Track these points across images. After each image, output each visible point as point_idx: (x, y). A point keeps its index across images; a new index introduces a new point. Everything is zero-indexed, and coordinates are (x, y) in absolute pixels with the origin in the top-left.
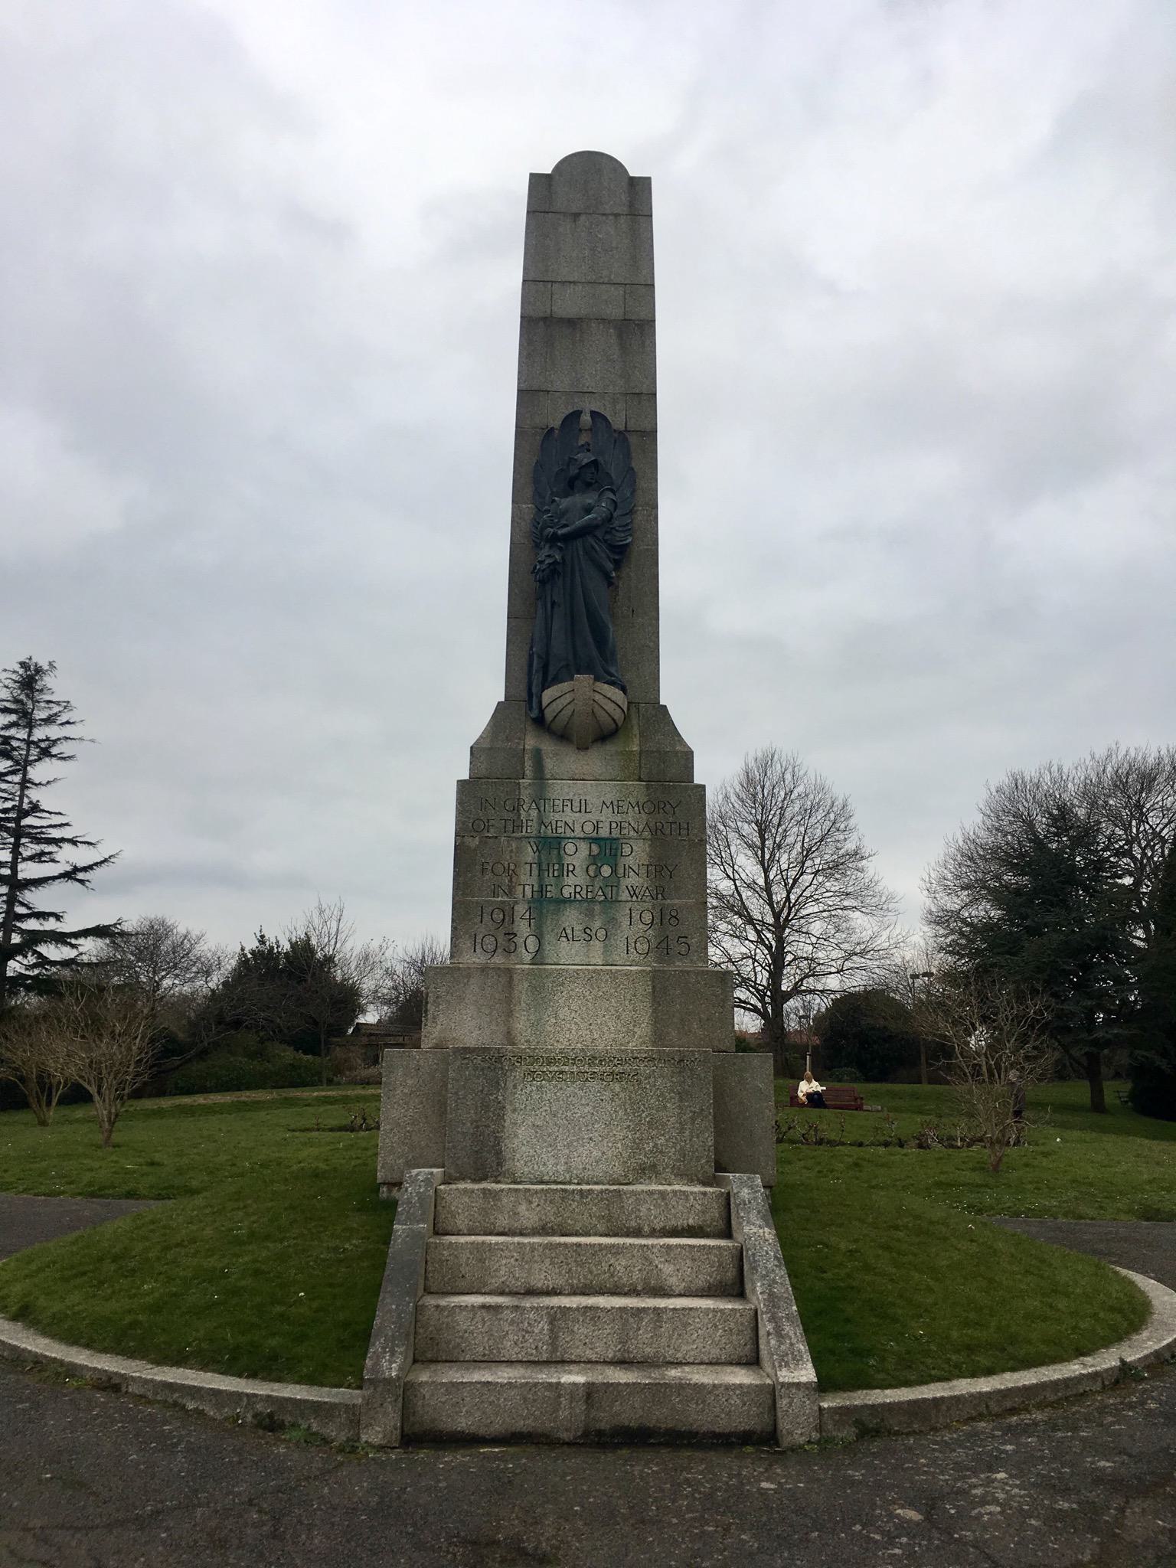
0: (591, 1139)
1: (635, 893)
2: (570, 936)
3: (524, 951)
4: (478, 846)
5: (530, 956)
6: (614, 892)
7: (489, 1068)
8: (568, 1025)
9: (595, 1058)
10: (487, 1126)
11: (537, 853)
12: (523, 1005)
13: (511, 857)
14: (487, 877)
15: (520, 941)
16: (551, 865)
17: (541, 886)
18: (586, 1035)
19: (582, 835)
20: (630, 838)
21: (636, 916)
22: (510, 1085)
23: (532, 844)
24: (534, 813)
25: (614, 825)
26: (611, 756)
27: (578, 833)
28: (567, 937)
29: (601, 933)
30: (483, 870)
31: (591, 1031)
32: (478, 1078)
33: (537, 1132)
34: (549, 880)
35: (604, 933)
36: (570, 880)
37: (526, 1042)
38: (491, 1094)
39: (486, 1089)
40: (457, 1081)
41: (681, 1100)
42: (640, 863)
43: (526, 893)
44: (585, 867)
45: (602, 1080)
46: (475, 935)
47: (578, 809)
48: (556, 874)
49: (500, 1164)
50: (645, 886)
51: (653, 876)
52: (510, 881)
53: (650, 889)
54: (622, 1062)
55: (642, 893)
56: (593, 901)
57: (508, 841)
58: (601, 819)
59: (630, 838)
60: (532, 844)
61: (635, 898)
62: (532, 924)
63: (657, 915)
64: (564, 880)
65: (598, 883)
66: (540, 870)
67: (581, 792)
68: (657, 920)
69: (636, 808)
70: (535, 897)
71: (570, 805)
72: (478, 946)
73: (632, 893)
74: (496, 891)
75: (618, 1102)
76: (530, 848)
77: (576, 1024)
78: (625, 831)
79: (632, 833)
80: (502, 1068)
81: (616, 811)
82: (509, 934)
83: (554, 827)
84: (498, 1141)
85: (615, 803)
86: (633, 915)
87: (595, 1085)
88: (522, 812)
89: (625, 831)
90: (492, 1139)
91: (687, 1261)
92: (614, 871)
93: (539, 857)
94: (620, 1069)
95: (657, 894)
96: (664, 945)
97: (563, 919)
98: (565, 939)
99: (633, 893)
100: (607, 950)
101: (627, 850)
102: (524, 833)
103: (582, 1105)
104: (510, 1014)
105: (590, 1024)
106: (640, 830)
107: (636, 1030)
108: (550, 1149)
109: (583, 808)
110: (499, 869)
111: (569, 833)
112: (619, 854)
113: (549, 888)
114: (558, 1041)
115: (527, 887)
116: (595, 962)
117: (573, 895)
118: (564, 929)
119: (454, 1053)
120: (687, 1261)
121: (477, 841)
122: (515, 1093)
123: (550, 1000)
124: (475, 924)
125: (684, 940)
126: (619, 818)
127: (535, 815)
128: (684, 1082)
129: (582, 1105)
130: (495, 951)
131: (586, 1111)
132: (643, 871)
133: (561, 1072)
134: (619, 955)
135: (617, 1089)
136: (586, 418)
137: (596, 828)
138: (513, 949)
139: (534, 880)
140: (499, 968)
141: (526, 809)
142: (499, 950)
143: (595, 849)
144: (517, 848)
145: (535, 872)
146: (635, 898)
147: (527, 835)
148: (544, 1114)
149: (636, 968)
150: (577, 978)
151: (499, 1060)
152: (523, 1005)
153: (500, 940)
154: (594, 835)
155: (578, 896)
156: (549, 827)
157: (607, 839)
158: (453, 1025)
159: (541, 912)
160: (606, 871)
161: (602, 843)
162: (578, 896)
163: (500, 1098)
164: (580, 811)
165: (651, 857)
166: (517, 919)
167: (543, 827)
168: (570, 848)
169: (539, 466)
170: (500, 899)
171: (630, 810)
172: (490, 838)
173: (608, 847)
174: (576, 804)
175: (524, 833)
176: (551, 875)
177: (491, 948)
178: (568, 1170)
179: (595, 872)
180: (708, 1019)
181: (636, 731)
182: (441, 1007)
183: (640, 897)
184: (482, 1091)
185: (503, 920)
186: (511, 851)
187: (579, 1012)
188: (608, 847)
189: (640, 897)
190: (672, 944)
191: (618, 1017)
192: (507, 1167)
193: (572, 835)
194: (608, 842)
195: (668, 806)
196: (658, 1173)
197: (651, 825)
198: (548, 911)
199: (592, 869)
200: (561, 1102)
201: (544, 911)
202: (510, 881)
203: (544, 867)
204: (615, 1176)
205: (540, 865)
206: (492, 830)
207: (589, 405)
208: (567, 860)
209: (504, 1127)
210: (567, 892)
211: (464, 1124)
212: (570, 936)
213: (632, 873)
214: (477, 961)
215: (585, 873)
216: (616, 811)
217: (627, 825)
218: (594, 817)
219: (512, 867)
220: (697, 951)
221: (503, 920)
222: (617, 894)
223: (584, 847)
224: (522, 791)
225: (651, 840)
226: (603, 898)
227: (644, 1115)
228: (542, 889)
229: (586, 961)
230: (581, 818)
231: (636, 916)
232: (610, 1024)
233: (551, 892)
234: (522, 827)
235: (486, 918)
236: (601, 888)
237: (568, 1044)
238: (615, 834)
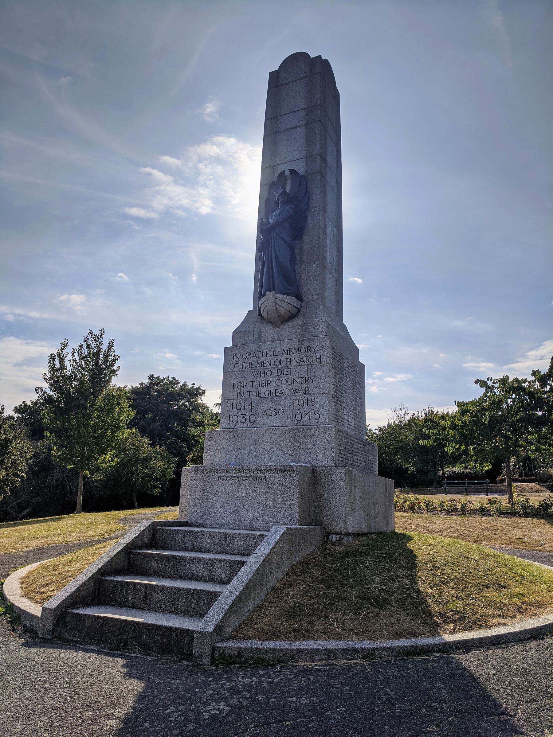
1: (296, 391)
2: (268, 414)
8: (261, 455)
25: (288, 360)
35: (282, 411)
54: (259, 471)
55: (299, 391)
58: (282, 358)
71: (269, 353)
73: (295, 391)
78: (292, 363)
81: (289, 354)
85: (289, 350)
86: (295, 402)
91: (229, 568)
94: (258, 475)
98: (266, 415)
106: (299, 361)
108: (228, 513)
109: (275, 353)
120: (229, 568)
125: (318, 412)
126: (289, 357)
135: (257, 485)
136: (287, 173)
155: (271, 394)
162: (271, 394)
169: (268, 200)
185: (241, 409)
190: (312, 415)
207: (286, 168)
216: (289, 354)
217: (293, 359)
218: (279, 358)
227: (267, 497)
232: (279, 454)
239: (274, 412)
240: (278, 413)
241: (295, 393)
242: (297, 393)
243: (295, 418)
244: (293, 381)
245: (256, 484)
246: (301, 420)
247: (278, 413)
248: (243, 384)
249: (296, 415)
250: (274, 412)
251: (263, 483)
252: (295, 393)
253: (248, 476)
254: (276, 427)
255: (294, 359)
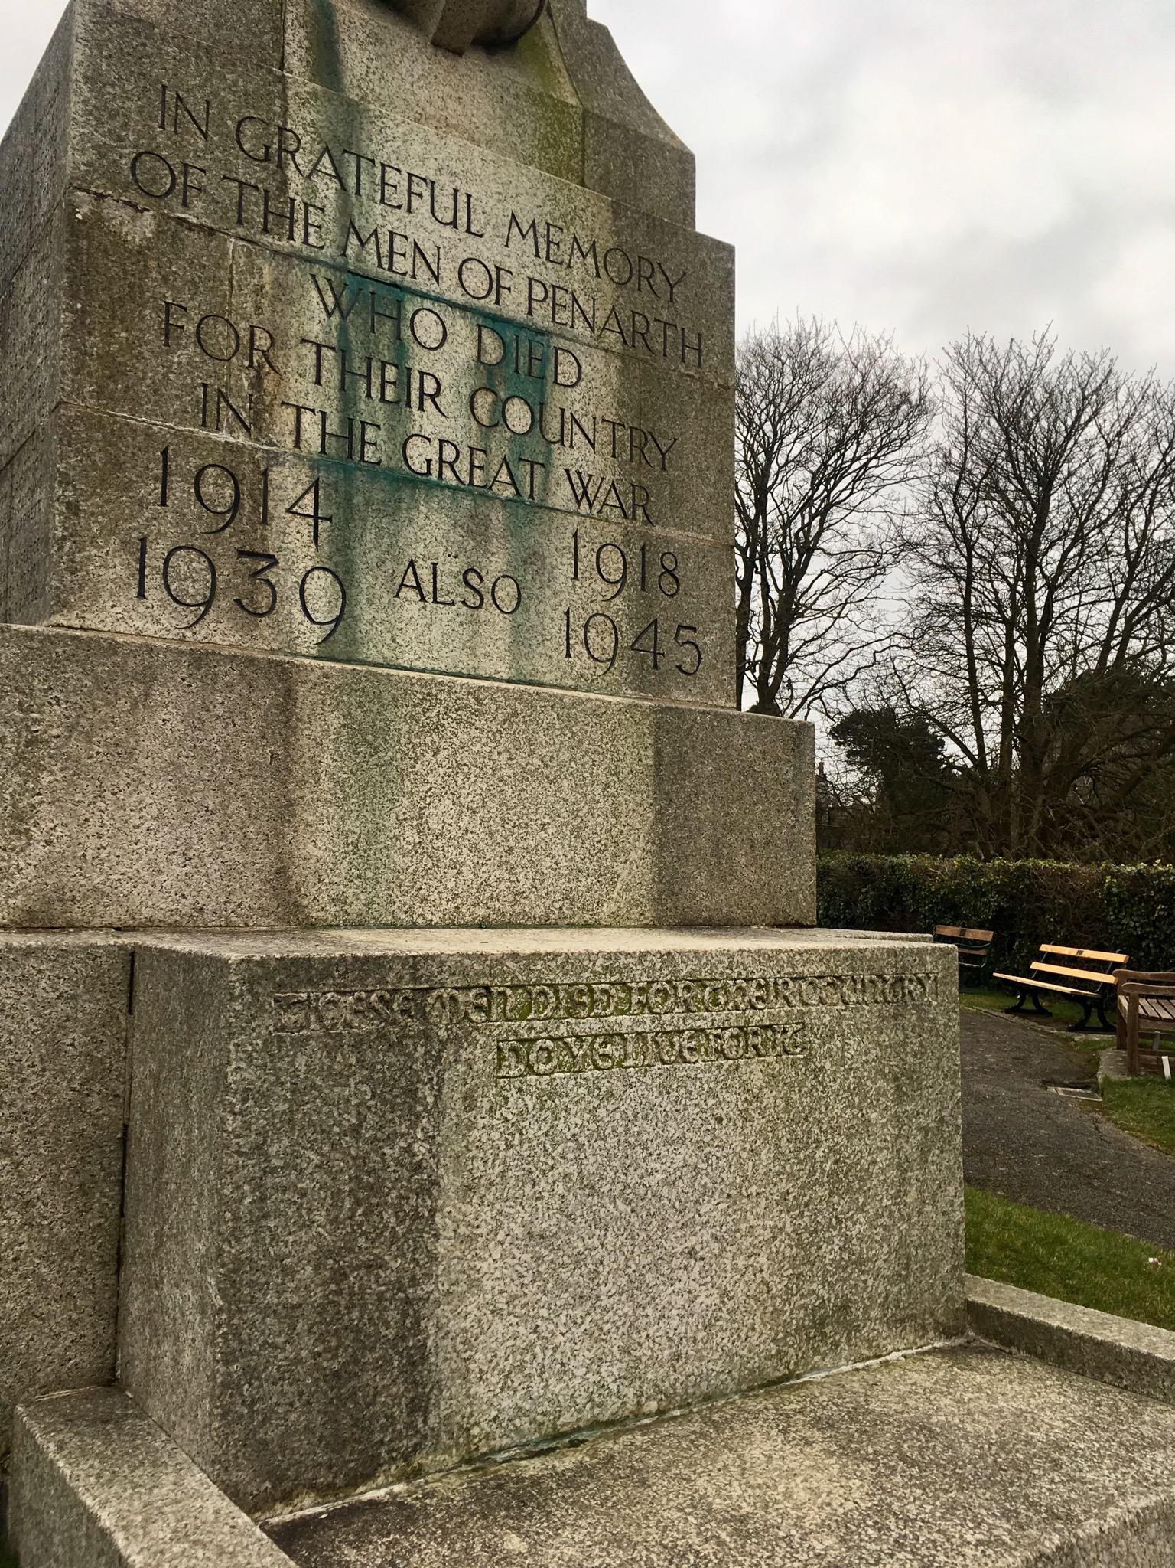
0: (691, 1253)
1: (585, 493)
2: (427, 587)
3: (299, 616)
4: (148, 246)
5: (317, 634)
6: (537, 480)
7: (382, 1036)
9: (701, 983)
10: (374, 1266)
11: (336, 318)
12: (327, 784)
13: (258, 308)
14: (179, 357)
15: (286, 581)
16: (375, 365)
17: (348, 422)
18: (499, 881)
19: (457, 296)
20: (574, 340)
21: (588, 560)
22: (453, 1098)
23: (322, 283)
24: (327, 190)
26: (517, 96)
27: (448, 287)
28: (418, 587)
29: (506, 591)
30: (169, 331)
31: (511, 872)
32: (341, 1078)
33: (539, 1259)
34: (371, 409)
35: (513, 590)
36: (426, 421)
37: (334, 900)
38: (390, 1139)
39: (372, 1119)
40: (263, 1097)
41: (900, 1097)
42: (598, 415)
43: (305, 436)
44: (466, 392)
45: (720, 1053)
46: (143, 541)
47: (449, 218)
48: (390, 395)
49: (419, 1406)
50: (609, 478)
51: (625, 457)
52: (257, 383)
53: (620, 488)
55: (601, 497)
56: (484, 494)
57: (249, 254)
59: (574, 340)
60: (322, 283)
61: (584, 505)
62: (323, 536)
63: (635, 561)
64: (410, 417)
65: (500, 447)
66: (344, 371)
67: (455, 166)
68: (634, 577)
69: (590, 260)
70: (331, 451)
71: (426, 194)
72: (153, 581)
73: (579, 491)
74: (211, 406)
75: (759, 1123)
76: (314, 293)
77: (473, 847)
78: (564, 316)
79: (580, 327)
80: (426, 1036)
82: (253, 555)
83: (385, 249)
84: (413, 1312)
86: (582, 552)
87: (701, 1070)
88: (291, 172)
89: (564, 316)
90: (392, 1315)
92: (538, 421)
93: (343, 331)
95: (634, 506)
96: (647, 642)
97: (409, 533)
98: (412, 595)
99: (582, 496)
100: (519, 640)
101: (567, 370)
102: (298, 242)
103: (668, 1142)
104: (285, 810)
105: (510, 851)
107: (618, 869)
108: (578, 1312)
109: (462, 215)
110: (220, 337)
111: (423, 281)
112: (550, 378)
113: (370, 434)
114: (424, 900)
115: (306, 417)
116: (490, 671)
117: (435, 467)
118: (412, 564)
119: (251, 982)
121: (147, 224)
122: (472, 1126)
123: (403, 773)
124: (142, 504)
125: (687, 635)
126: (549, 274)
127: (332, 194)
128: (904, 1044)
129: (668, 1142)
130: (208, 604)
131: (679, 1161)
132: (603, 437)
133: (609, 1037)
134: (548, 662)
135: (758, 1079)
137: (496, 286)
138: (264, 603)
139: (323, 398)
140: (252, 661)
141: (306, 169)
142: (223, 604)
143: (493, 352)
144: (277, 283)
145: (331, 374)
146: (584, 505)
147: (305, 251)
148: (560, 1189)
149: (619, 699)
150: (475, 713)
151: (417, 1004)
152: (327, 784)
153: (225, 572)
154: (489, 304)
155: (448, 474)
156: (371, 246)
157: (522, 326)
158: (93, 842)
159: (349, 499)
160: (519, 416)
161: (509, 335)
162: (448, 474)
163: (421, 1149)
164: (454, 224)
165: (621, 404)
166: (278, 511)
167: (354, 240)
168: (427, 327)
170: (223, 436)
171: (576, 260)
172: (191, 227)
173: (524, 349)
174: (444, 200)
175: (298, 242)
176: (375, 393)
177: (195, 590)
178: (632, 1375)
179: (492, 412)
180: (768, 843)
181: (558, 62)
182: (45, 778)
183: (597, 506)
184: (355, 1131)
185: (236, 506)
186: (259, 290)
187: (482, 812)
188: (524, 349)
189: (597, 506)
190: (666, 642)
191: (577, 831)
192: (444, 1409)
193: (434, 288)
194: (523, 334)
195: (659, 278)
196: (851, 1328)
197: (622, 316)
198: (368, 503)
199: (484, 401)
200: (612, 1141)
201: (358, 500)
202: (257, 383)
203: (358, 365)
204: (755, 1362)
205: (344, 353)
206: (199, 205)
208: (420, 361)
209: (433, 1258)
210: (420, 454)
211: (288, 1272)
212: (427, 587)
213: (578, 437)
214: (151, 628)
215: (465, 410)
216: (543, 253)
219: (262, 341)
220: (714, 667)
221: (236, 506)
222: (545, 490)
223: (462, 329)
224: (293, 107)
225: (622, 357)
226: (509, 492)
227: (819, 1154)
228: (350, 433)
229: (466, 663)
230: (455, 245)
231: (588, 560)
232: (557, 851)
233: (377, 449)
234: (293, 222)
235: (180, 490)
236: (505, 460)
237: (451, 907)
238: (541, 317)
239: (467, 584)
240: (488, 599)
241: (579, 502)
242: (591, 505)
243: (579, 648)
244: (567, 427)
245: (754, 1072)
246: (612, 660)
247: (488, 599)
248: (244, 335)
249: (586, 631)
250: (467, 584)
251: (794, 1064)
252: (579, 502)
253: (701, 1024)
254: (411, 669)
255: (575, 300)
